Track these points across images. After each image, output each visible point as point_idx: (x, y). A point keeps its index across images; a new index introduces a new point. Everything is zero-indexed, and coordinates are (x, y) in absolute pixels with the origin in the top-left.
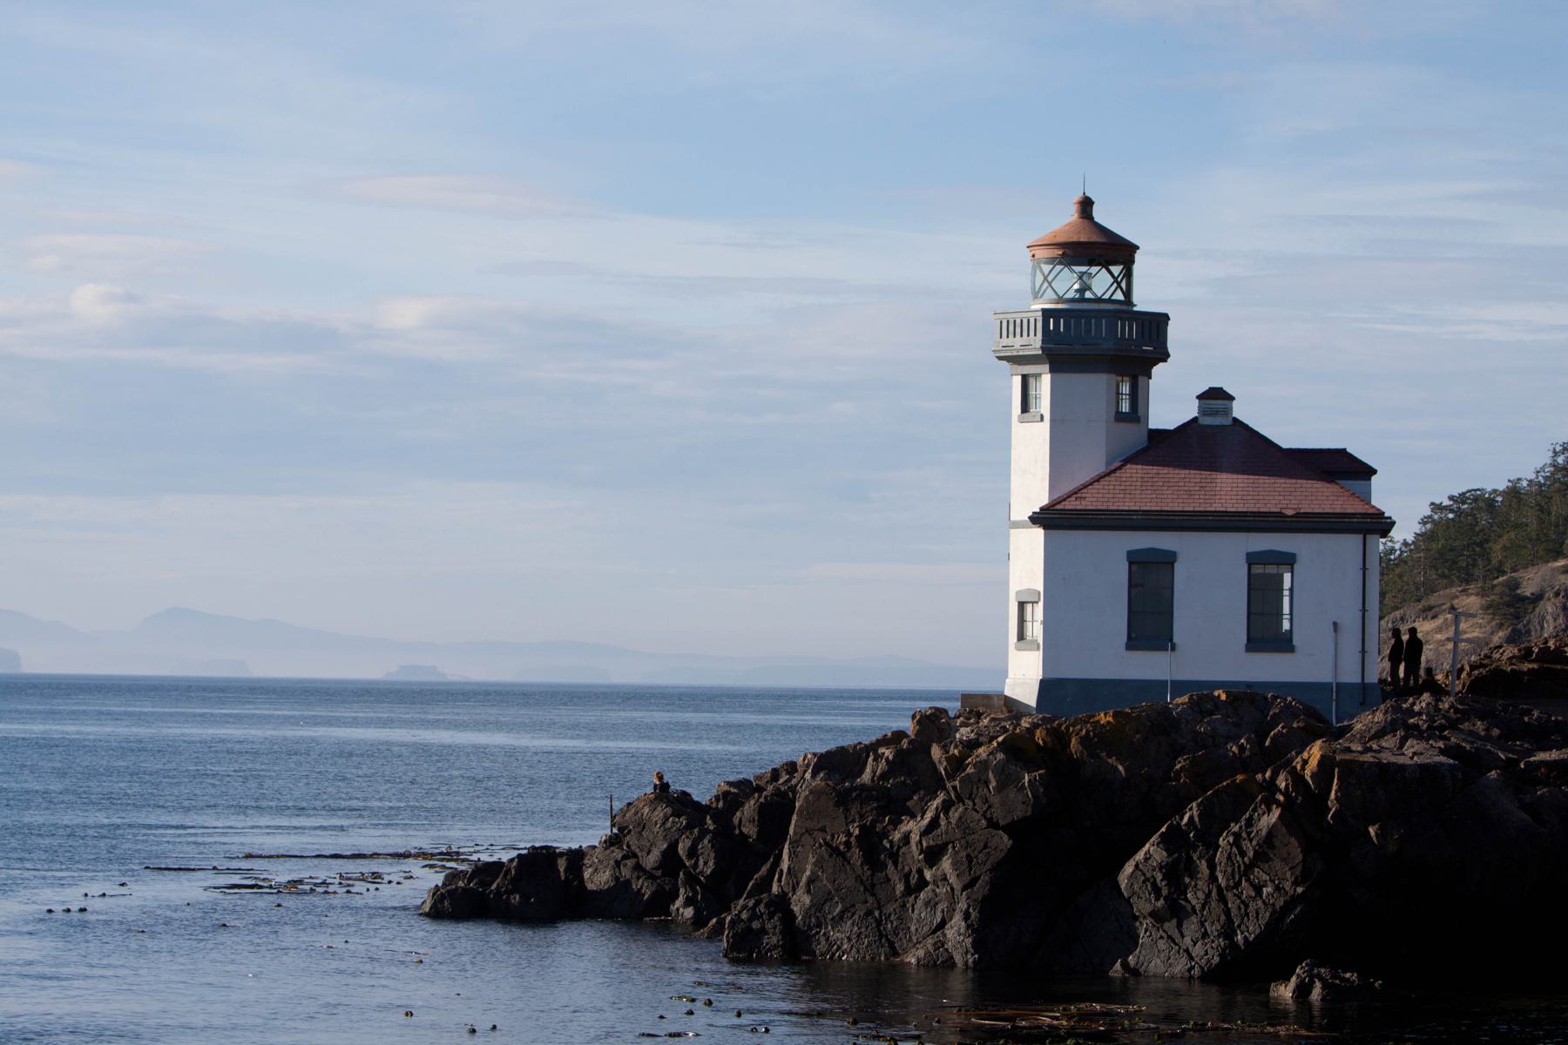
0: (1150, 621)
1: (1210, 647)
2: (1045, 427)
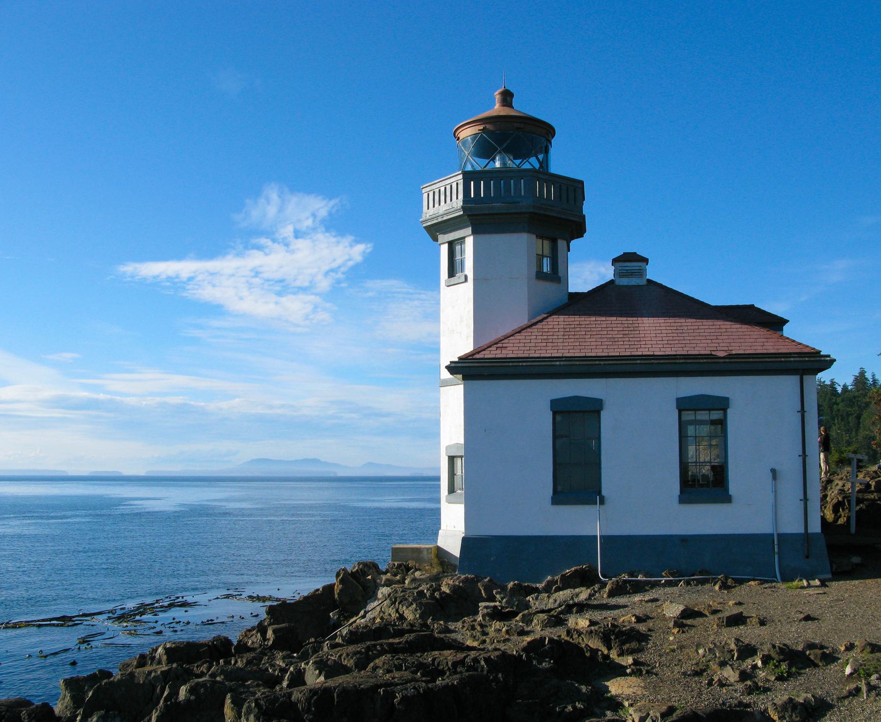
0: (577, 474)
1: (640, 496)
2: (469, 286)
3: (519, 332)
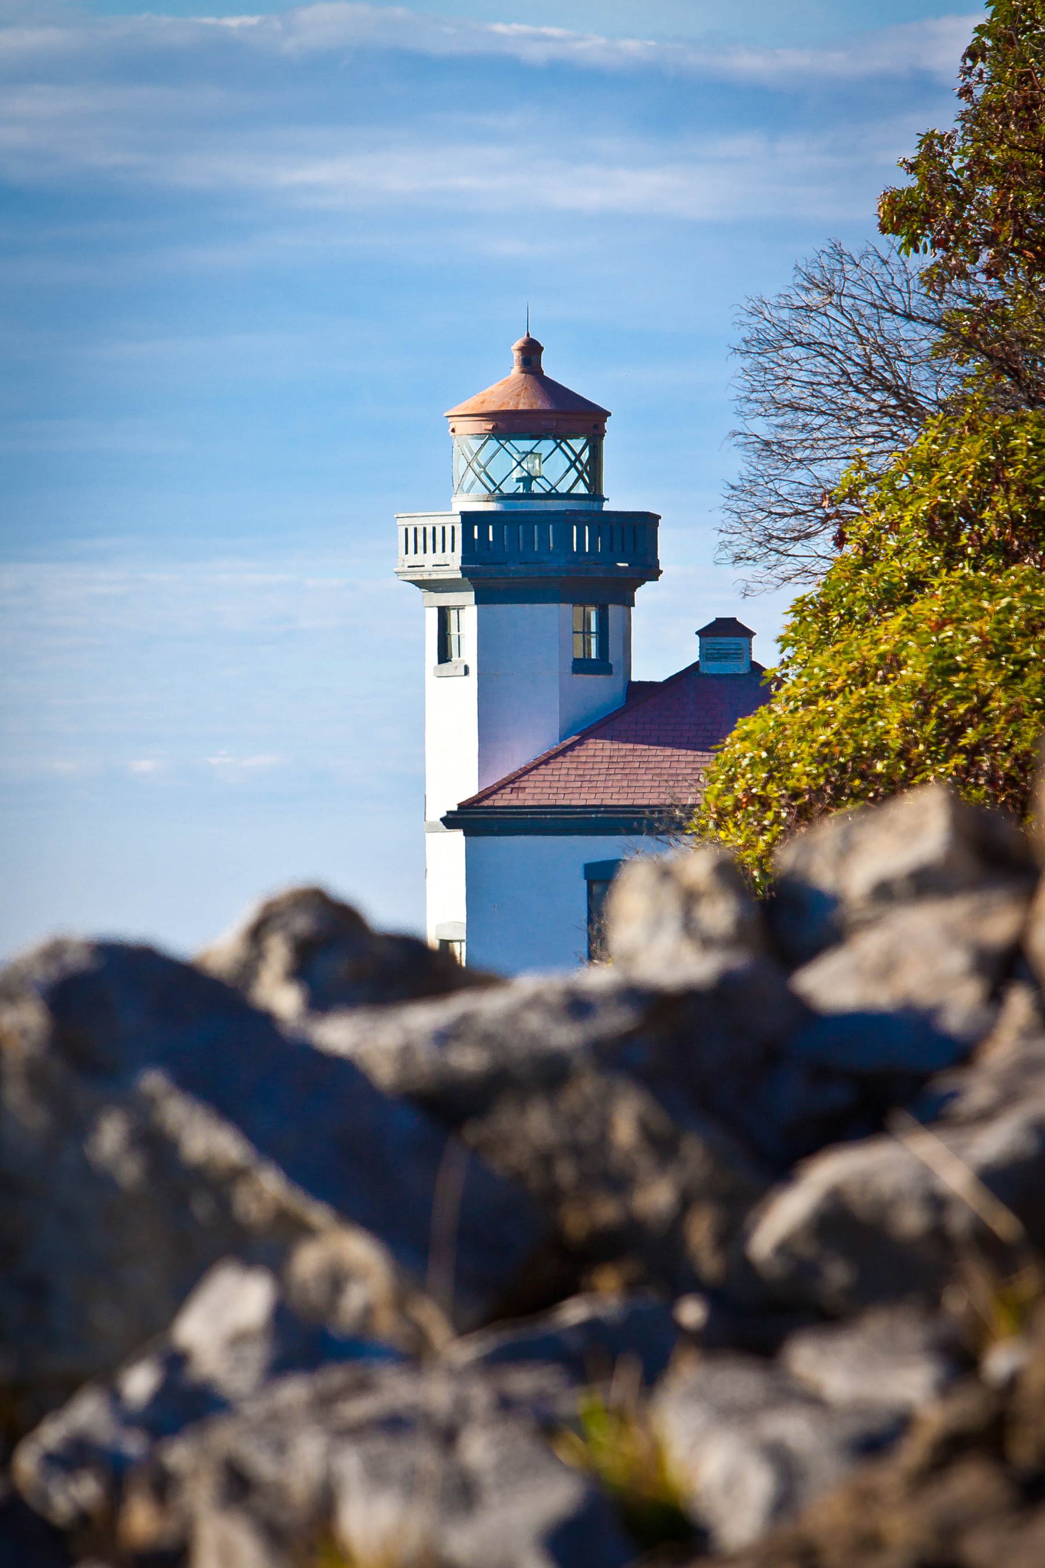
2: (472, 681)
3: (546, 762)
